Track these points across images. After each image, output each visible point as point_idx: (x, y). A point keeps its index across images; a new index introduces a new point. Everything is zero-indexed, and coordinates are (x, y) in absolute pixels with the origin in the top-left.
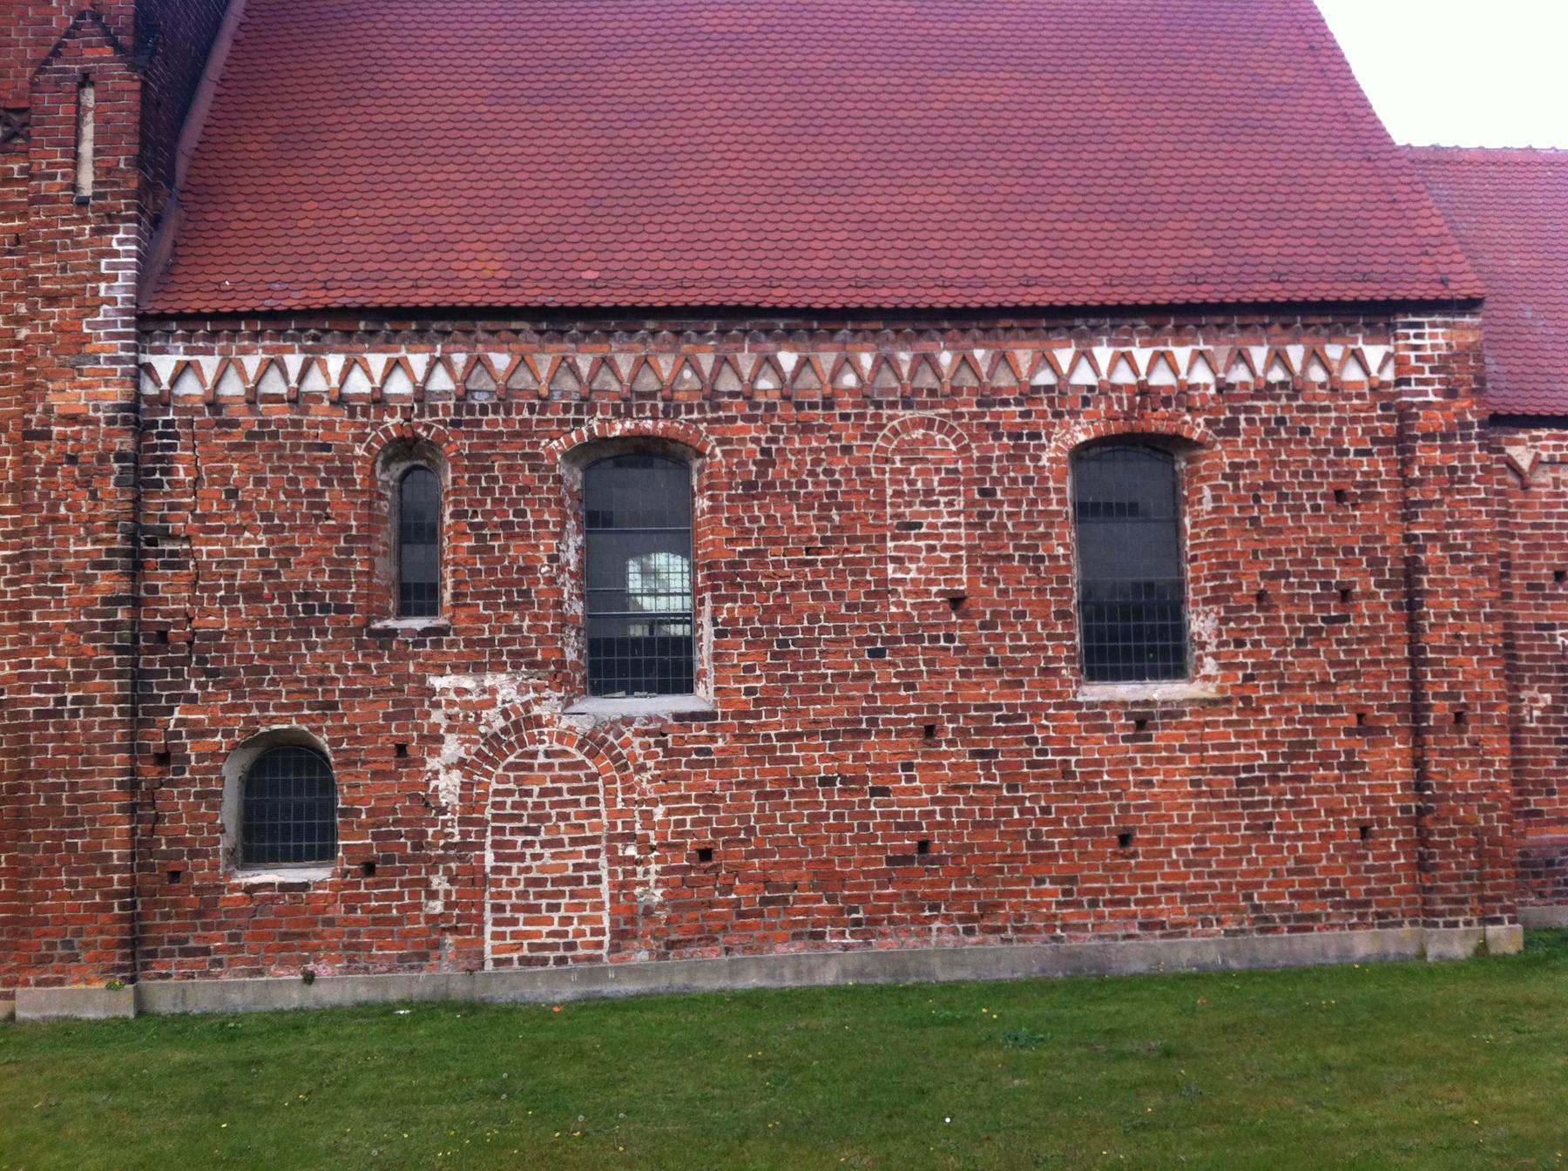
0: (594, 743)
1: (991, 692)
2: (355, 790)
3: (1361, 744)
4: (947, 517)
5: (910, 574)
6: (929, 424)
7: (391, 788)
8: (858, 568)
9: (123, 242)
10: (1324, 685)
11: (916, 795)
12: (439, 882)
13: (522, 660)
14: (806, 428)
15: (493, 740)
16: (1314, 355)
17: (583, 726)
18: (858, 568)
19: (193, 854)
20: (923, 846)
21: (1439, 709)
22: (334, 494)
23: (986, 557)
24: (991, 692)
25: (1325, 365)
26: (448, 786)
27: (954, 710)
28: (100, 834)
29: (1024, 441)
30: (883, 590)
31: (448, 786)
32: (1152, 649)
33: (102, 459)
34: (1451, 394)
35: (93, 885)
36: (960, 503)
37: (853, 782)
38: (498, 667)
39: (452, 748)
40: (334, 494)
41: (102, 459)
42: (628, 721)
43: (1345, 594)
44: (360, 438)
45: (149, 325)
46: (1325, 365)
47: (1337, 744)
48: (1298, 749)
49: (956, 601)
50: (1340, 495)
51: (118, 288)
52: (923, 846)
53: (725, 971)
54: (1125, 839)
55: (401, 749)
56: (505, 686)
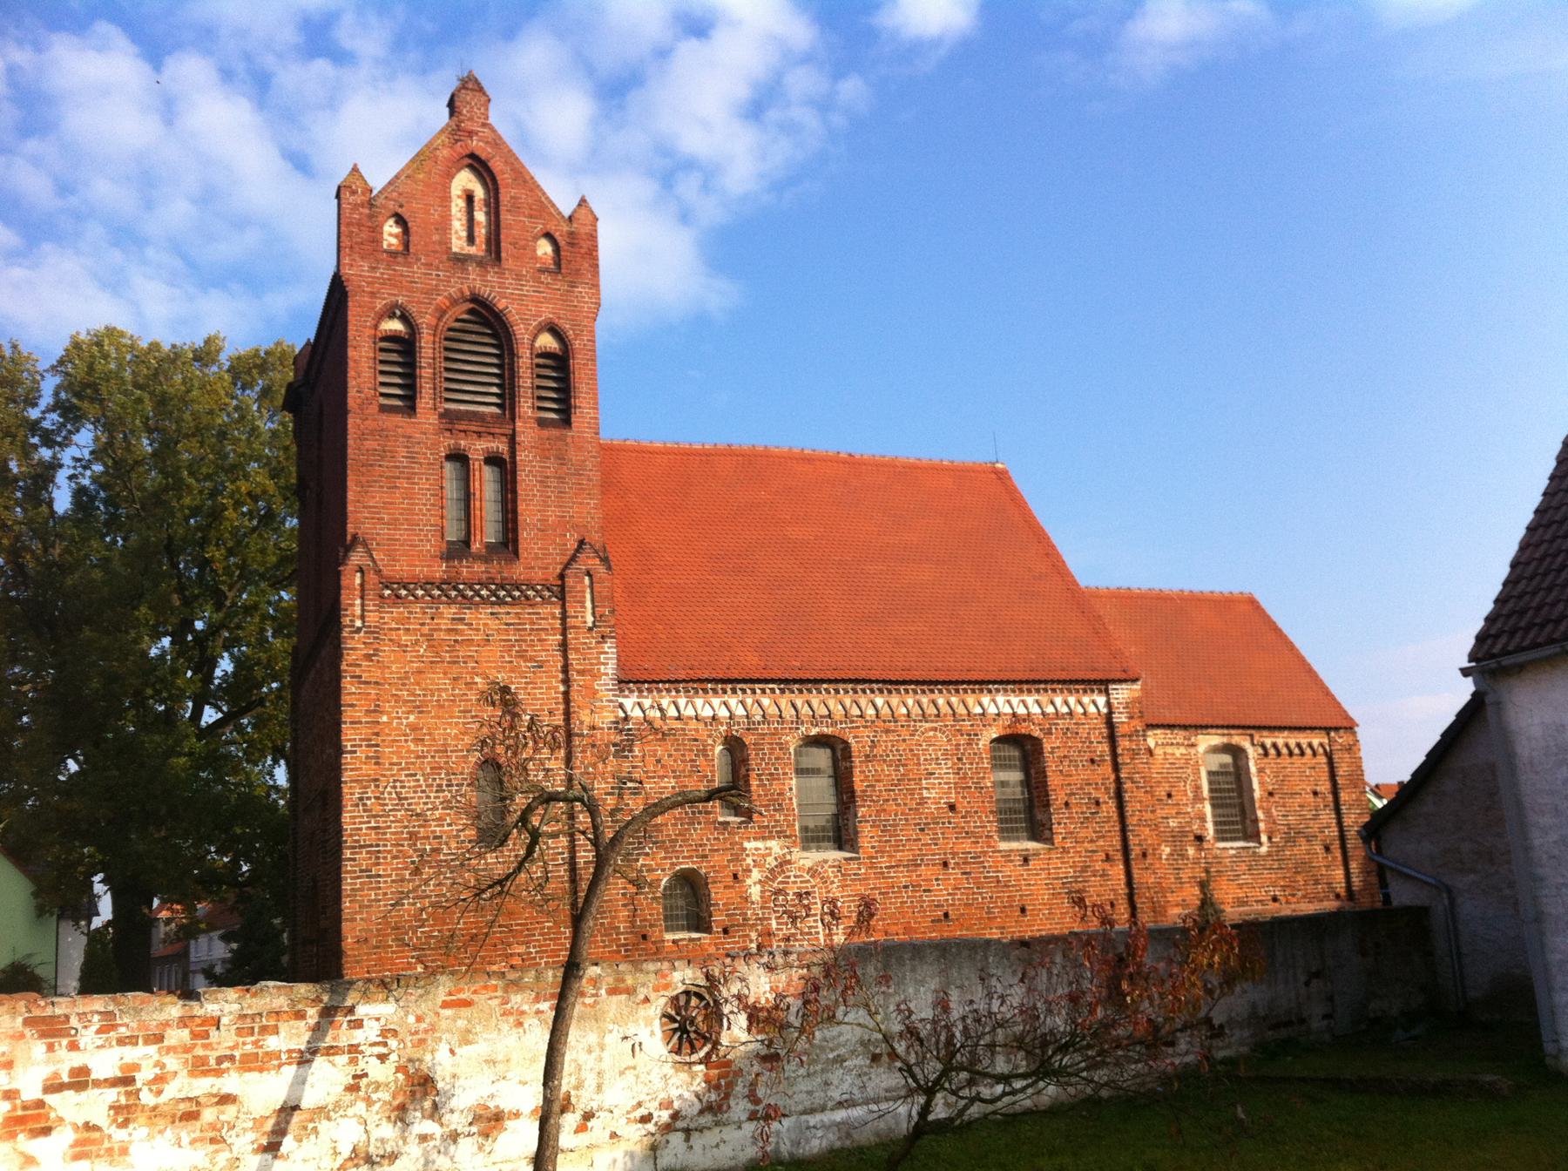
0: (813, 872)
1: (967, 846)
2: (719, 894)
3: (1107, 866)
4: (945, 769)
5: (935, 794)
6: (935, 729)
7: (730, 893)
8: (911, 792)
9: (609, 647)
10: (1092, 841)
11: (941, 893)
12: (754, 935)
13: (781, 834)
14: (887, 731)
15: (772, 871)
16: (690, 702)
17: (808, 864)
18: (911, 792)
19: (651, 926)
20: (946, 915)
21: (1135, 852)
22: (701, 761)
23: (962, 786)
24: (967, 846)
25: (981, 705)
26: (755, 892)
27: (954, 854)
28: (613, 918)
29: (972, 737)
30: (923, 801)
31: (755, 892)
32: (362, 617)
33: (607, 746)
34: (1131, 718)
35: (611, 941)
36: (950, 764)
37: (916, 886)
38: (771, 838)
39: (756, 875)
40: (701, 761)
41: (607, 746)
42: (826, 861)
43: (1098, 803)
44: (710, 736)
45: (624, 682)
46: (981, 705)
47: (1098, 866)
48: (1084, 869)
49: (952, 807)
50: (1092, 761)
51: (610, 668)
52: (946, 915)
53: (177, 212)
54: (1023, 910)
55: (735, 876)
56: (775, 846)
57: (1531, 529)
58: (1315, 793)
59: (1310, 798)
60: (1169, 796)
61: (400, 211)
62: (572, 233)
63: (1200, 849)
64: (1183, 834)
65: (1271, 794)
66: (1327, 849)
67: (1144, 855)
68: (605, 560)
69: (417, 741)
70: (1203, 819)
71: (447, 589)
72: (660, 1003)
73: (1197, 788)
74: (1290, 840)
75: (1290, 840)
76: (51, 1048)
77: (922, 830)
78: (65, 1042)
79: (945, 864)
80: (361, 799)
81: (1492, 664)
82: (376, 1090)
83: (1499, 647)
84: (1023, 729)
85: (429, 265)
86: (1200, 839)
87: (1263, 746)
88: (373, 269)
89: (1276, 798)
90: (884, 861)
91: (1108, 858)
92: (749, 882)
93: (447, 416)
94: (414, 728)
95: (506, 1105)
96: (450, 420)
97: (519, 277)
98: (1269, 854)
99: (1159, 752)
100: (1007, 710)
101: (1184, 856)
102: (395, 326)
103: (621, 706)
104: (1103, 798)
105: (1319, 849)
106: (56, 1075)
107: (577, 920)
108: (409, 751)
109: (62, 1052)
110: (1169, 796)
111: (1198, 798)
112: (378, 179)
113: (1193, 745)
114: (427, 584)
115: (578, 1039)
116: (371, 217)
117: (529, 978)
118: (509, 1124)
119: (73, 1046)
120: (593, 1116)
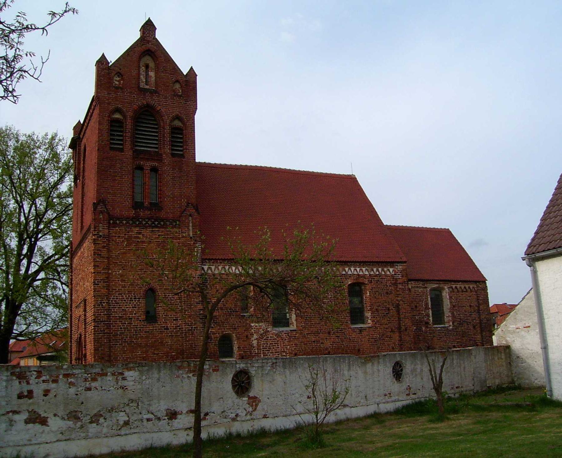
3: (392, 334)
13: (266, 321)
15: (261, 335)
26: (255, 343)
31: (255, 343)
34: (402, 276)
39: (255, 336)
42: (283, 331)
43: (389, 309)
47: (389, 334)
48: (383, 335)
50: (387, 293)
55: (247, 336)
56: (263, 325)
57: (548, 207)
58: (470, 306)
59: (469, 308)
60: (416, 307)
61: (120, 71)
62: (186, 81)
63: (427, 327)
64: (421, 322)
65: (454, 306)
66: (474, 327)
67: (406, 330)
68: (197, 210)
69: (123, 281)
70: (428, 316)
71: (135, 221)
72: (230, 377)
73: (427, 304)
74: (461, 324)
75: (461, 324)
76: (20, 383)
77: (321, 319)
78: (25, 381)
79: (329, 333)
80: (101, 303)
81: (533, 256)
82: (132, 402)
83: (534, 250)
84: (361, 280)
85: (131, 93)
86: (427, 323)
87: (452, 287)
88: (109, 94)
89: (456, 308)
90: (306, 332)
91: (392, 331)
92: (253, 339)
93: (135, 151)
94: (122, 276)
95: (178, 409)
96: (137, 154)
97: (166, 97)
98: (453, 329)
99: (413, 290)
100: (355, 273)
101: (421, 330)
102: (117, 116)
103: (203, 268)
104: (391, 307)
105: (471, 327)
106: (22, 393)
107: (57, 441)
108: (120, 285)
109: (24, 384)
110: (416, 307)
111: (427, 308)
112: (112, 58)
113: (426, 287)
114: (127, 218)
115: (205, 383)
116: (109, 74)
117: (185, 364)
118: (179, 416)
119: (28, 383)
120: (208, 414)
